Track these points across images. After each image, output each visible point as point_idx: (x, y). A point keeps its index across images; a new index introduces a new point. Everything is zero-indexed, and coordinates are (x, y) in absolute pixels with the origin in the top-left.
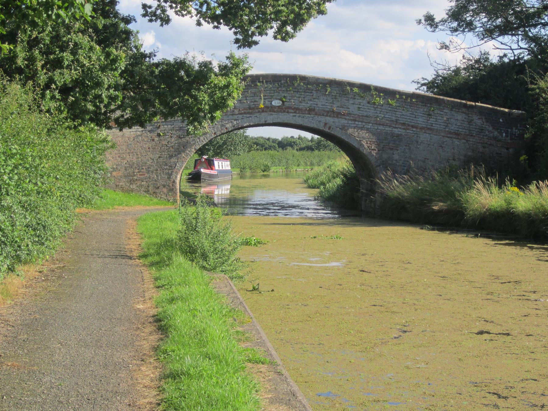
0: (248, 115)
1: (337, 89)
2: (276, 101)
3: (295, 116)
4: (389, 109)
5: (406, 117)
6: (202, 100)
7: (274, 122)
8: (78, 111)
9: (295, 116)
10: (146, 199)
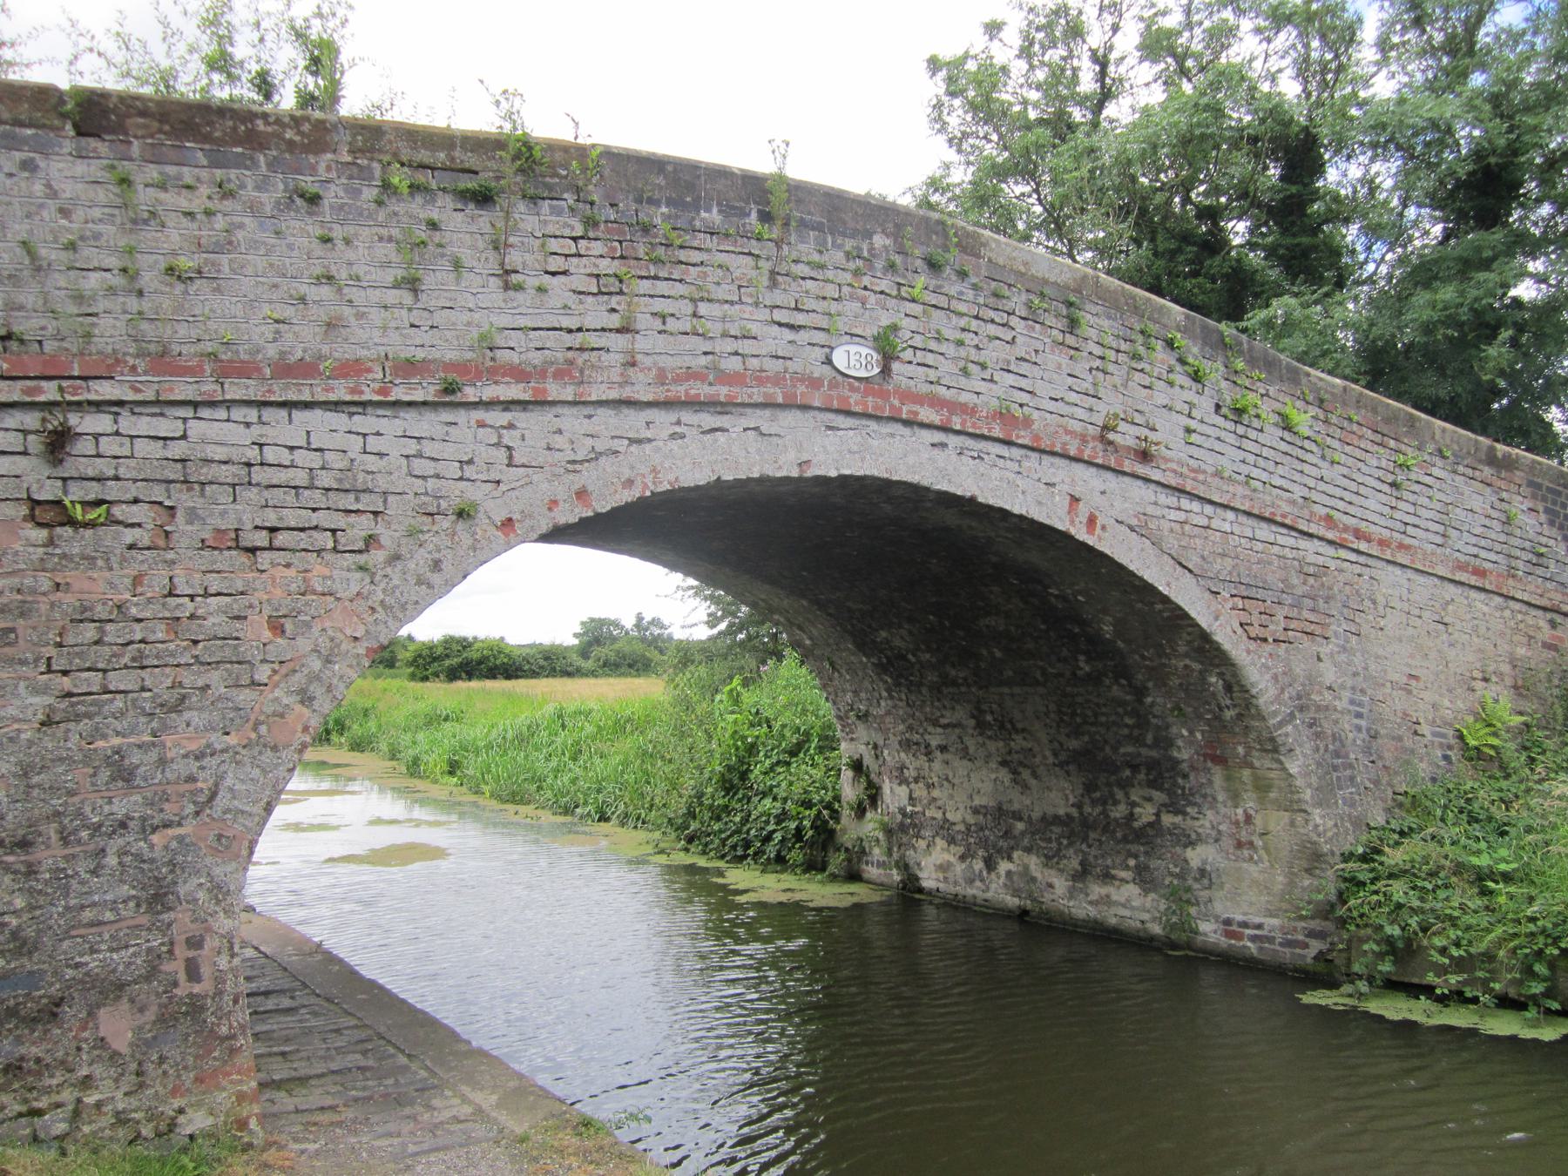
0: (708, 420)
1: (1106, 323)
2: (853, 349)
3: (943, 445)
4: (1283, 446)
5: (1330, 489)
6: (39, 931)
7: (847, 472)
8: (16, 1086)
9: (943, 445)
10: (550, 680)
